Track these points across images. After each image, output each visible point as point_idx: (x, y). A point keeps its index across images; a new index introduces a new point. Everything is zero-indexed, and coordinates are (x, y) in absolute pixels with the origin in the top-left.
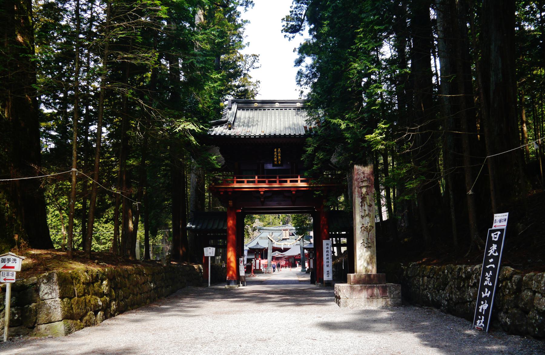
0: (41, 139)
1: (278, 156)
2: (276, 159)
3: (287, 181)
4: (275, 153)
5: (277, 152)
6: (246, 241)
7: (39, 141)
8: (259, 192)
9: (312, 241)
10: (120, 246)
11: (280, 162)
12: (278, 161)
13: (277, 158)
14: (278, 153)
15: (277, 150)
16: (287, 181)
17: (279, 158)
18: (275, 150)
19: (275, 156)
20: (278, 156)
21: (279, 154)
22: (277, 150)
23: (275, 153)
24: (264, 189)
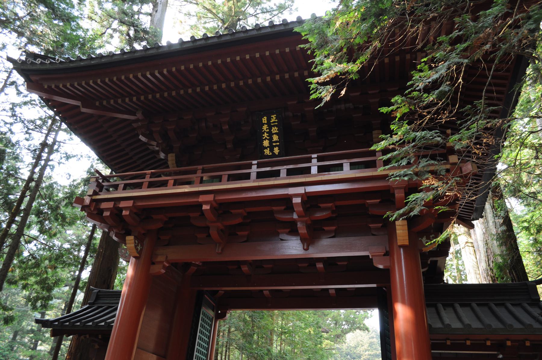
0: (121, 260)
1: (270, 134)
2: (266, 143)
3: (279, 171)
4: (265, 127)
5: (269, 123)
6: (69, 344)
7: (116, 262)
8: (200, 205)
9: (118, 277)
10: (343, 329)
11: (265, 120)
12: (271, 148)
13: (271, 140)
14: (270, 127)
15: (269, 119)
16: (279, 171)
17: (275, 138)
18: (265, 120)
19: (266, 135)
20: (270, 134)
21: (275, 130)
22: (269, 119)
23: (265, 127)
24: (210, 197)
